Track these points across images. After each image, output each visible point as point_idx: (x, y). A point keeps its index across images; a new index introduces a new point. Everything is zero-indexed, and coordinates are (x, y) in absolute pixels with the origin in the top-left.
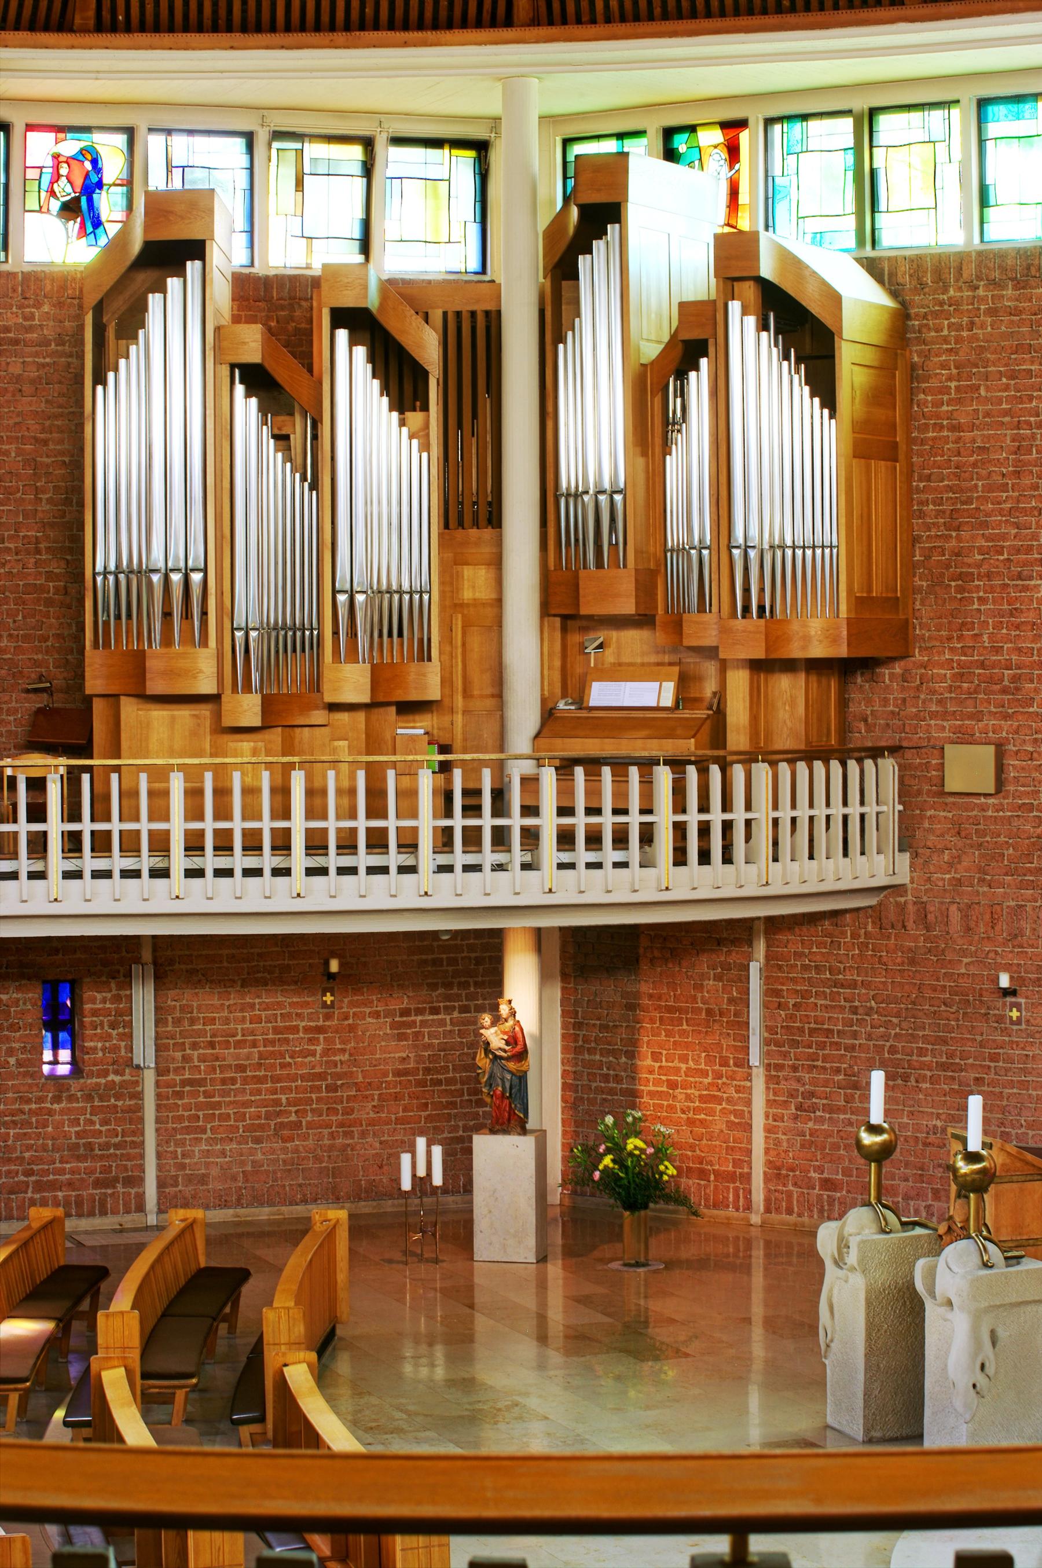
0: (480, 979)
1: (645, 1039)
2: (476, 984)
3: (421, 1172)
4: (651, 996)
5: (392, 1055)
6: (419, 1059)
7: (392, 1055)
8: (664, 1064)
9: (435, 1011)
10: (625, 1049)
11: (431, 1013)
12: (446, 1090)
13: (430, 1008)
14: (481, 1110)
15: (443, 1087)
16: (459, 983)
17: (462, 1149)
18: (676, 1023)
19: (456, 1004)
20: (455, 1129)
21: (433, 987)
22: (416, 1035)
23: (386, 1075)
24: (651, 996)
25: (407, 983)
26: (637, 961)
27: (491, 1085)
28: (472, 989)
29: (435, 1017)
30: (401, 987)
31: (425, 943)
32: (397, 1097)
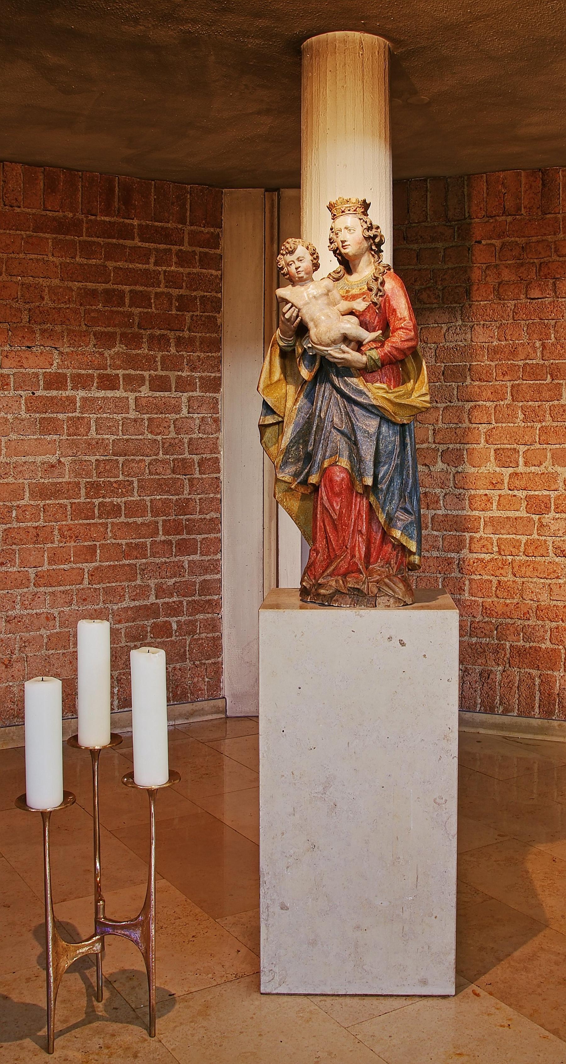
0: (186, 334)
1: (483, 428)
2: (179, 342)
3: (95, 735)
4: (494, 352)
5: (30, 459)
6: (80, 468)
7: (30, 459)
8: (521, 469)
9: (109, 383)
10: (442, 447)
11: (100, 387)
12: (127, 524)
13: (100, 377)
14: (186, 559)
15: (122, 519)
16: (152, 338)
17: (155, 626)
18: (546, 395)
19: (146, 374)
20: (143, 591)
21: (106, 340)
22: (75, 422)
23: (17, 493)
24: (494, 352)
25: (58, 328)
26: (468, 292)
27: (309, 458)
28: (173, 350)
29: (110, 394)
30: (48, 334)
31: (93, 262)
32: (38, 536)
